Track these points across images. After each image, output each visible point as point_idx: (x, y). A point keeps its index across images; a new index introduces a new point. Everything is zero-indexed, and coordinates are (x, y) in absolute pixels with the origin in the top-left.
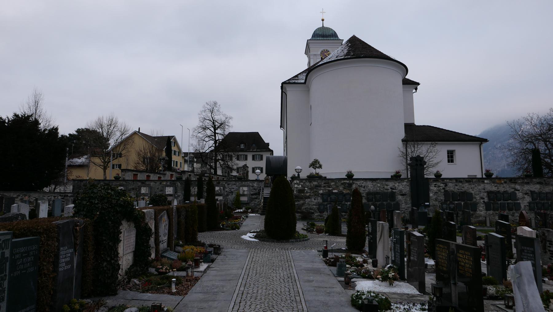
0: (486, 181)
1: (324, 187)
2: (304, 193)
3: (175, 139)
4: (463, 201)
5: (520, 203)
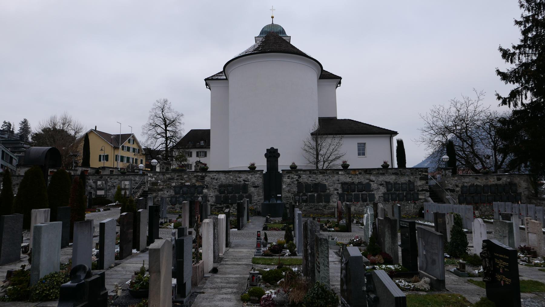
0: (340, 173)
1: (177, 179)
2: (157, 186)
3: (134, 137)
4: (317, 192)
5: (374, 194)
